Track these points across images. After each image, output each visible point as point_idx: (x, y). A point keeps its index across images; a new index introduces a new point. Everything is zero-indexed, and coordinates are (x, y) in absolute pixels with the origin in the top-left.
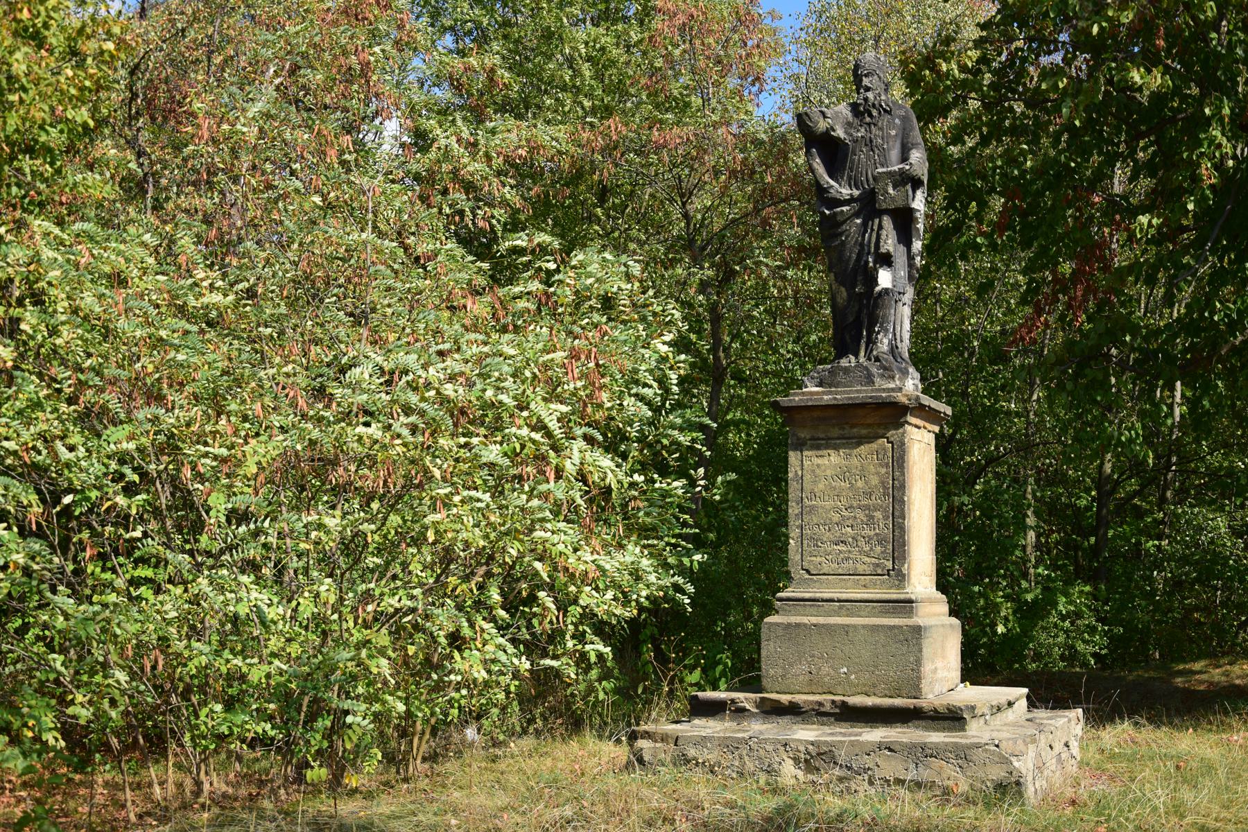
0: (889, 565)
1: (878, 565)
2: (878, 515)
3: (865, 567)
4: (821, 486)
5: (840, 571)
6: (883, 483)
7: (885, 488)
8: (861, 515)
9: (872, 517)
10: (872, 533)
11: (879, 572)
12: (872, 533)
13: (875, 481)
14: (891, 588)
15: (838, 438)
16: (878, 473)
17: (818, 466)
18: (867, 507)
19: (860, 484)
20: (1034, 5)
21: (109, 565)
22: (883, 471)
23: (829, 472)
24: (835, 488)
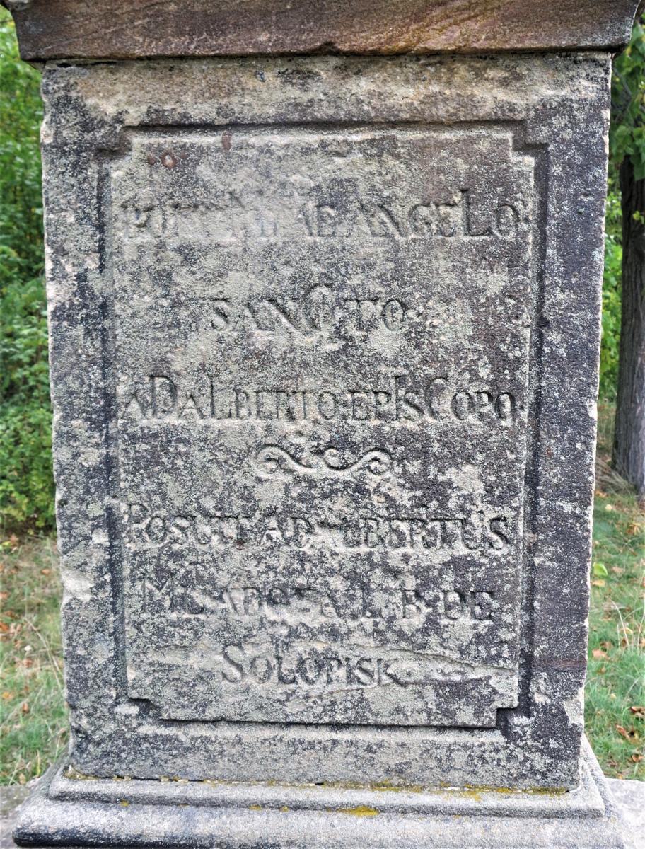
0: (507, 688)
1: (458, 691)
2: (467, 479)
3: (404, 697)
4: (202, 345)
5: (293, 709)
6: (490, 337)
7: (500, 362)
8: (387, 479)
9: (439, 491)
10: (439, 556)
11: (466, 715)
12: (439, 556)
13: (452, 326)
14: (508, 785)
15: (283, 124)
16: (470, 293)
17: (188, 253)
18: (413, 447)
19: (385, 341)
20: (3, 120)
21: (71, 649)
22: (496, 282)
23: (237, 284)
24: (264, 358)
